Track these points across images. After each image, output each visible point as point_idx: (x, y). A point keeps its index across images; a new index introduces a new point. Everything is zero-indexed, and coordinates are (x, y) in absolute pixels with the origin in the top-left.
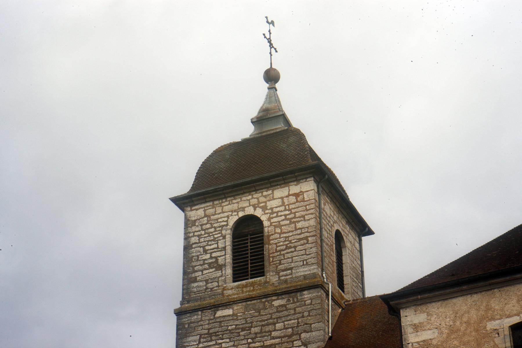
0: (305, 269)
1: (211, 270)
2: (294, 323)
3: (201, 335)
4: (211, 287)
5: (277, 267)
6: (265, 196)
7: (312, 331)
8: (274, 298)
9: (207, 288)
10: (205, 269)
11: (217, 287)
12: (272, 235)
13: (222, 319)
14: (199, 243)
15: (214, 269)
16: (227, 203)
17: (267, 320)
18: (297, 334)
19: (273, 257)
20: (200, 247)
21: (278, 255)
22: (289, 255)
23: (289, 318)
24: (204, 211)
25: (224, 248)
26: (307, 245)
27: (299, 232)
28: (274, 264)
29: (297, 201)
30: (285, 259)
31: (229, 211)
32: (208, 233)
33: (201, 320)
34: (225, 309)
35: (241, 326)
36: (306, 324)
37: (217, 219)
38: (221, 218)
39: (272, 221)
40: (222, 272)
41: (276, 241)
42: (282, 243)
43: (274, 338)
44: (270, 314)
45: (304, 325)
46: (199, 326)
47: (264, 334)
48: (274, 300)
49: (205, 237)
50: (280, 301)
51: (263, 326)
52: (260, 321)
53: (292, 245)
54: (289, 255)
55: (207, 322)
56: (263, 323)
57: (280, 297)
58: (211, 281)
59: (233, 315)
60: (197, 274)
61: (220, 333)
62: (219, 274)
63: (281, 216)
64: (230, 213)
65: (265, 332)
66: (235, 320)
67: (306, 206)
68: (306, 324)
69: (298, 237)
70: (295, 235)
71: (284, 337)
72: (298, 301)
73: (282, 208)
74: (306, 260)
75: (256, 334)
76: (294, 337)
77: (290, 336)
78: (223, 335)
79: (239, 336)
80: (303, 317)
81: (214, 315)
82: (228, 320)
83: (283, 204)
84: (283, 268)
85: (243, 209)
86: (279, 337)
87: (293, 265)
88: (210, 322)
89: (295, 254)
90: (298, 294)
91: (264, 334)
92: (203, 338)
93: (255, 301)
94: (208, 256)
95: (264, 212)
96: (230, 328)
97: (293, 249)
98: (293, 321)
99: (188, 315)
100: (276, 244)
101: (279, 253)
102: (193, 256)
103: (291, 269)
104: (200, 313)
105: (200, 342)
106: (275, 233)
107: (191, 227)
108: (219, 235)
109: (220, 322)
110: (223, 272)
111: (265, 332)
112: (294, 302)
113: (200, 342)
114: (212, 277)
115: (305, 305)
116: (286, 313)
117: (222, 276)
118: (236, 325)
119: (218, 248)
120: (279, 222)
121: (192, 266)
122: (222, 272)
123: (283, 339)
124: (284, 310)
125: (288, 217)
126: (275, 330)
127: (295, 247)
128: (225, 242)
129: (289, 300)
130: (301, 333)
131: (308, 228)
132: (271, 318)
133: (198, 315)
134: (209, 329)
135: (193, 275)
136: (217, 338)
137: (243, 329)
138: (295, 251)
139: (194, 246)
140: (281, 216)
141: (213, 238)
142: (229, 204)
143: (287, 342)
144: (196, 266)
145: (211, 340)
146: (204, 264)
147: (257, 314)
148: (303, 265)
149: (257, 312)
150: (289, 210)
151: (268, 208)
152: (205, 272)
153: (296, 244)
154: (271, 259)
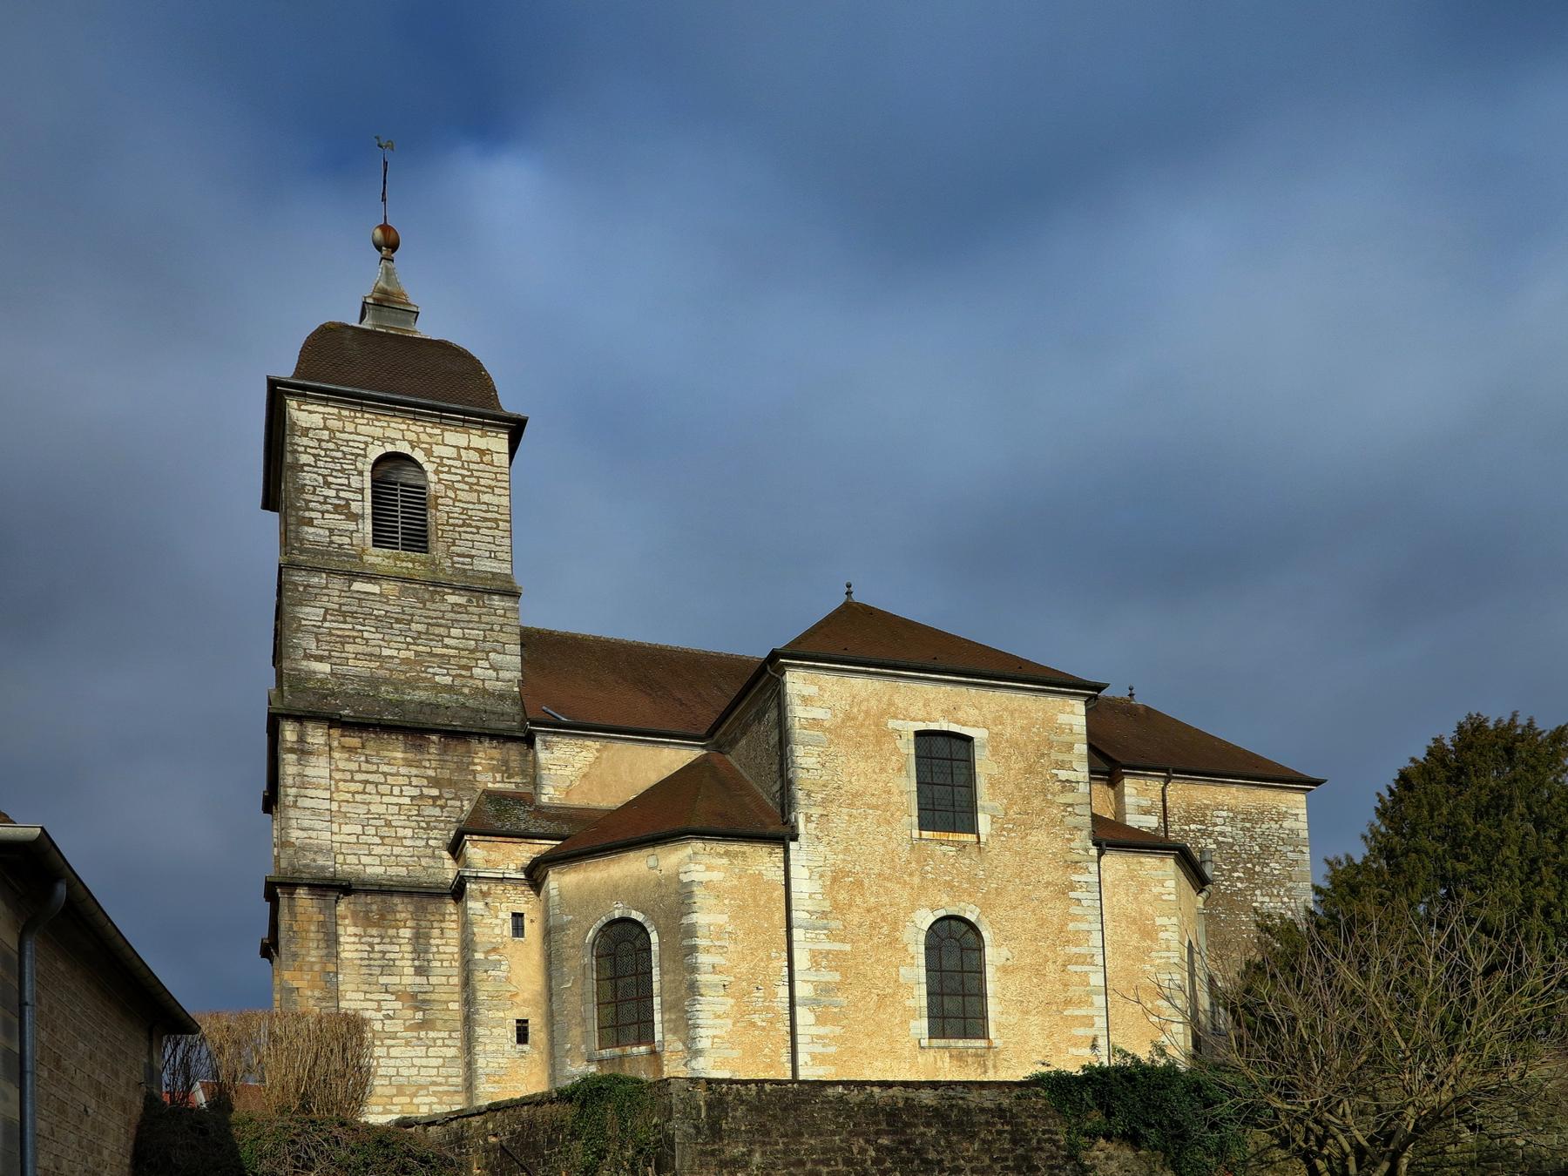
0: (495, 565)
1: (337, 517)
2: (478, 635)
3: (327, 610)
4: (340, 542)
5: (449, 547)
6: (430, 435)
7: (506, 654)
8: (446, 590)
9: (331, 542)
10: (328, 512)
11: (348, 544)
12: (442, 497)
13: (362, 596)
14: (316, 467)
15: (343, 517)
16: (365, 421)
17: (435, 618)
18: (483, 651)
19: (442, 530)
20: (319, 475)
21: (450, 531)
22: (469, 537)
23: (471, 625)
24: (323, 418)
25: (362, 491)
26: (497, 531)
27: (484, 507)
28: (444, 542)
29: (482, 462)
30: (461, 539)
31: (369, 436)
32: (331, 457)
33: (326, 588)
34: (367, 583)
35: (396, 616)
36: (498, 642)
37: (347, 441)
38: (354, 441)
39: (441, 476)
40: (357, 525)
41: (447, 509)
42: (456, 515)
43: (447, 647)
44: (441, 611)
45: (493, 642)
46: (324, 595)
47: (431, 637)
48: (449, 594)
49: (326, 462)
50: (457, 597)
51: (428, 624)
52: (425, 617)
53: (474, 524)
54: (469, 537)
55: (337, 593)
56: (430, 621)
57: (457, 592)
58: (339, 533)
59: (381, 595)
60: (313, 515)
61: (359, 615)
62: (352, 526)
63: (456, 474)
64: (371, 440)
65: (433, 634)
66: (384, 603)
67: (496, 473)
68: (498, 642)
69: (483, 515)
70: (479, 510)
71: (463, 650)
72: (486, 607)
73: (458, 464)
74: (495, 552)
75: (419, 633)
76: (479, 655)
77: (472, 651)
78: (364, 620)
79: (392, 628)
80: (492, 630)
81: (350, 587)
82: (373, 601)
83: (459, 458)
84: (458, 552)
85: (393, 441)
86: (456, 648)
87: (474, 552)
88: (343, 594)
89: (477, 537)
90: (486, 597)
91: (431, 637)
92: (331, 615)
93: (417, 586)
94: (333, 493)
95: (428, 458)
96: (375, 612)
97: (474, 530)
98: (477, 632)
99: (304, 573)
100: (447, 512)
101: (452, 528)
102: (306, 485)
103: (472, 557)
104: (324, 575)
105: (325, 620)
106: (447, 497)
107: (300, 437)
108: (353, 467)
109: (360, 599)
110: (360, 527)
111: (433, 634)
112: (478, 606)
113: (325, 620)
114: (341, 528)
115: (495, 615)
116: (465, 617)
117: (357, 531)
118: (387, 612)
119: (349, 485)
120: (453, 482)
121: (304, 500)
122: (357, 525)
123: (461, 652)
124: (462, 613)
125: (466, 479)
126: (449, 636)
127: (478, 528)
128: (363, 481)
129: (469, 601)
130: (490, 652)
131: (498, 506)
132: (443, 618)
133: (322, 578)
134: (340, 605)
135: (307, 514)
136: (353, 621)
137: (398, 621)
138: (478, 533)
139: (306, 468)
140: (456, 474)
141: (340, 468)
142: (368, 424)
143: (468, 658)
144: (311, 501)
145: (345, 622)
146: (325, 503)
147: (421, 605)
148: (490, 557)
149: (420, 603)
150: (468, 470)
151: (435, 454)
152: (326, 516)
153: (479, 524)
154: (440, 533)
